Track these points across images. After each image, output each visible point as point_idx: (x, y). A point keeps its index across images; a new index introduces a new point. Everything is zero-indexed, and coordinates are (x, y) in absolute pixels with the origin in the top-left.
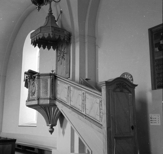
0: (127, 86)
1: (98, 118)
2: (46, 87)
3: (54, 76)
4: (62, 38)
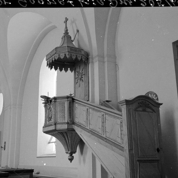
0: (150, 105)
1: (119, 140)
2: (63, 111)
3: (71, 99)
4: (79, 59)
